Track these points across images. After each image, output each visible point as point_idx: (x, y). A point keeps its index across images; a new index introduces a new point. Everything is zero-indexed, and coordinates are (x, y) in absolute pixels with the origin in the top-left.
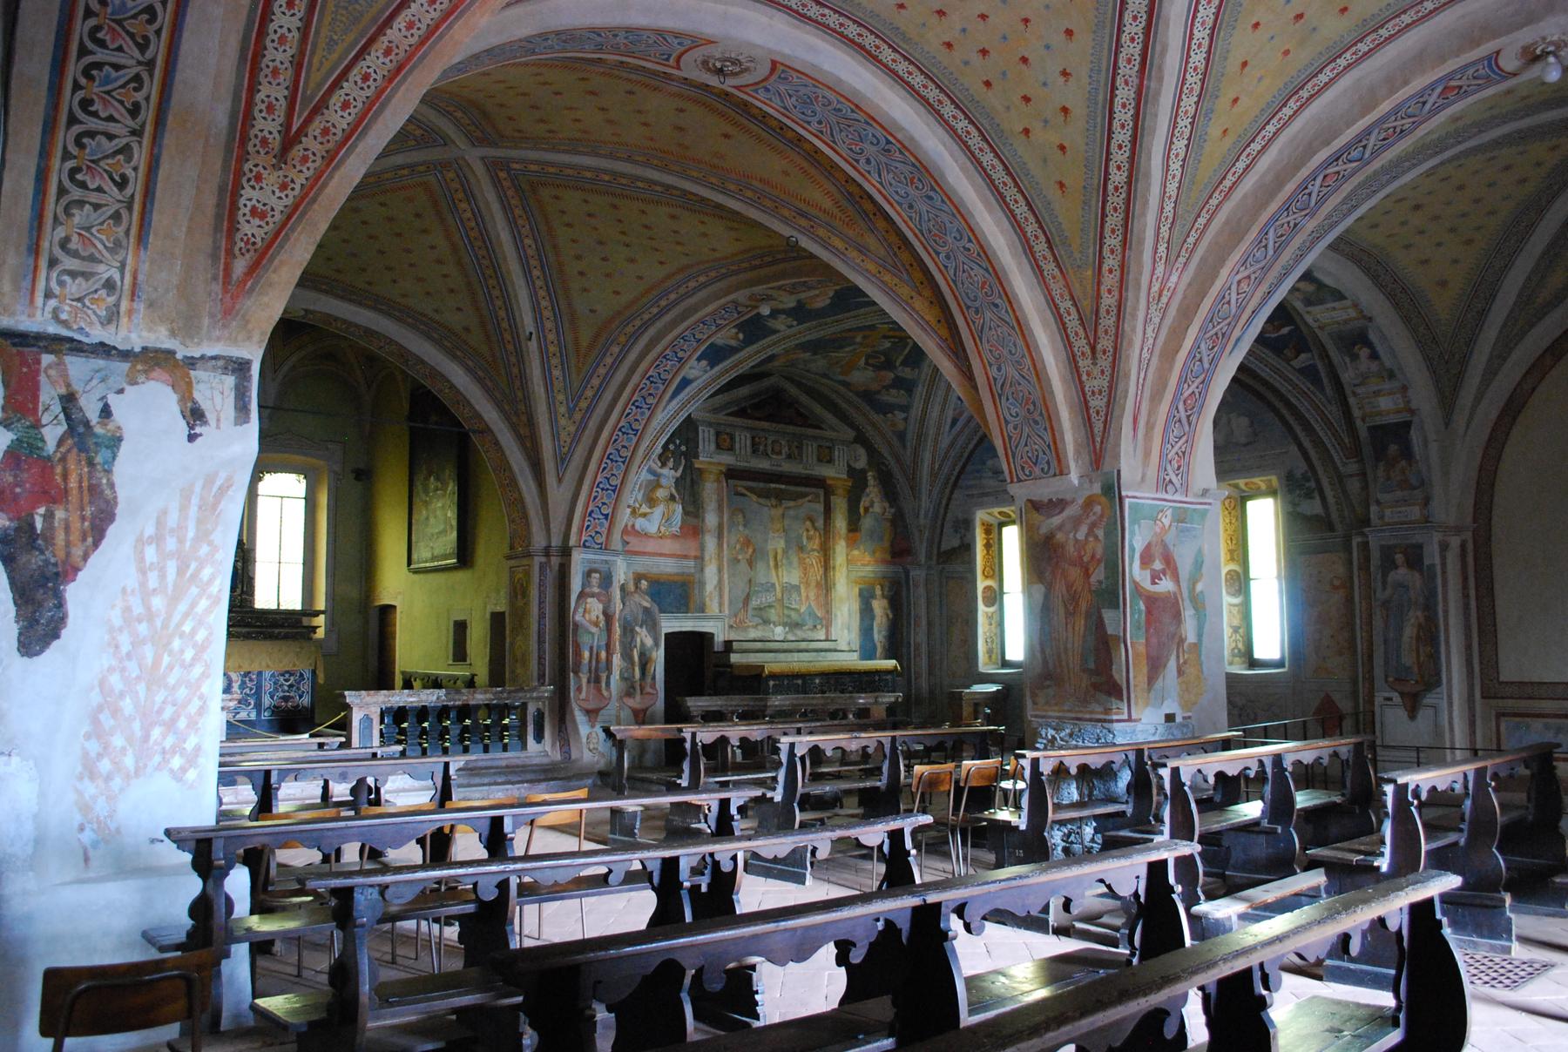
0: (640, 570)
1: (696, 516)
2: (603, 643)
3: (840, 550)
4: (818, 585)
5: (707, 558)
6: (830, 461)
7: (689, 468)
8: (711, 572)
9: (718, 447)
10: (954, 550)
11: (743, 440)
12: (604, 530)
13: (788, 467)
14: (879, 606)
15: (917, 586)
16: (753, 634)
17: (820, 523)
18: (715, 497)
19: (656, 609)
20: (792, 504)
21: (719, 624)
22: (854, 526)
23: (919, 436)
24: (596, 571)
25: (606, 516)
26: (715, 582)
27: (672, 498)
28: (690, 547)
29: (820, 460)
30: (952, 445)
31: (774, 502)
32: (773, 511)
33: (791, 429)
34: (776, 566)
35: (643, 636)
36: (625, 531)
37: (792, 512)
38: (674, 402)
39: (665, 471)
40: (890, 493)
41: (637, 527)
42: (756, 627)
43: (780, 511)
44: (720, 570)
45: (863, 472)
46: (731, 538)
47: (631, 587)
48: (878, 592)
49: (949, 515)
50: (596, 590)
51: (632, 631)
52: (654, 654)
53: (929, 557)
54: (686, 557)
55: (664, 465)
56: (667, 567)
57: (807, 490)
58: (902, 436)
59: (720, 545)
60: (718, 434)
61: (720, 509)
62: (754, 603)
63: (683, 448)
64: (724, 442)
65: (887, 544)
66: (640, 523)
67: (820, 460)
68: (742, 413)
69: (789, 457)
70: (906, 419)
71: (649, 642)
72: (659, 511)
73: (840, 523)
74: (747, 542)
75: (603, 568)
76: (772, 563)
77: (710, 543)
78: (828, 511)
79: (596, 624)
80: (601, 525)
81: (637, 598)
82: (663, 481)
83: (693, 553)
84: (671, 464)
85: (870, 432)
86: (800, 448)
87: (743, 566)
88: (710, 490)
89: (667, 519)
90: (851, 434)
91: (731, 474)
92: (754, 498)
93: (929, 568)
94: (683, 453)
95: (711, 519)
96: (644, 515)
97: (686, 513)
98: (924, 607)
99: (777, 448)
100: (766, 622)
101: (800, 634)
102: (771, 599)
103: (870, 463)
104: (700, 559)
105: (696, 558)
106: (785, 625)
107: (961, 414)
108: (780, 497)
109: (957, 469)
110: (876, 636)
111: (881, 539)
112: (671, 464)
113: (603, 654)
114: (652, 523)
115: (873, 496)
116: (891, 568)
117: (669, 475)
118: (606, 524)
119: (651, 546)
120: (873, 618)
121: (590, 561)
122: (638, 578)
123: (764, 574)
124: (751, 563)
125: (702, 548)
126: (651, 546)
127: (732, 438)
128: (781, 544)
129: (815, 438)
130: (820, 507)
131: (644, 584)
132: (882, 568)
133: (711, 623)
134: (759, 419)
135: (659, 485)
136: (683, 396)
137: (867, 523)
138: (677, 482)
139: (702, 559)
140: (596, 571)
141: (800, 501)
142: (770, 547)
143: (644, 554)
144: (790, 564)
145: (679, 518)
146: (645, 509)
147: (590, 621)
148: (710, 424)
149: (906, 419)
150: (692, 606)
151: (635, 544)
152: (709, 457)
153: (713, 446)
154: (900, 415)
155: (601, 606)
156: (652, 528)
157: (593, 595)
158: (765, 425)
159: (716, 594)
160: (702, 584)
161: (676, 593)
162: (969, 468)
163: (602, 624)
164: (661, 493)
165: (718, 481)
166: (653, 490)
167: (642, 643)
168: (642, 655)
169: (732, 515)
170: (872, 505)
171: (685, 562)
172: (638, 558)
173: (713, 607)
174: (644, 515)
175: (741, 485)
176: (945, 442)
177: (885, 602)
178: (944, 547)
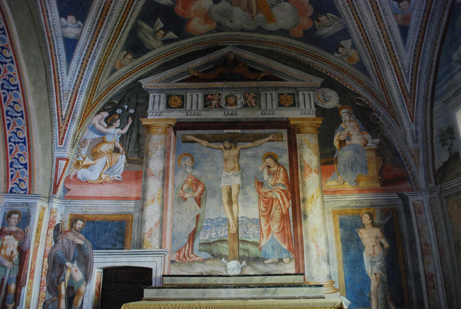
0: (78, 211)
1: (140, 163)
2: (14, 276)
3: (311, 183)
4: (284, 217)
5: (149, 197)
6: (294, 105)
7: (136, 125)
8: (152, 212)
9: (168, 106)
10: (446, 165)
11: (194, 99)
12: (26, 178)
13: (242, 115)
14: (370, 237)
15: (419, 211)
16: (199, 269)
17: (284, 159)
18: (160, 147)
19: (88, 245)
20: (249, 144)
21: (159, 260)
22: (328, 158)
23: (374, 58)
24: (15, 212)
25: (25, 165)
26: (156, 218)
27: (116, 150)
28: (132, 190)
29: (280, 105)
30: (417, 58)
31: (227, 144)
32: (226, 153)
33: (246, 84)
34: (230, 203)
35: (74, 271)
36: (68, 180)
37: (249, 152)
38: (74, 63)
39: (112, 130)
40: (368, 121)
41: (79, 176)
42: (203, 261)
43: (234, 152)
44: (163, 208)
45: (335, 111)
46: (178, 180)
47: (66, 226)
48: (366, 219)
49: (435, 131)
50: (14, 228)
51: (62, 267)
52: (83, 288)
53: (428, 180)
54: (126, 199)
55: (110, 125)
56: (106, 208)
57: (267, 131)
58: (361, 66)
59: (165, 186)
60: (168, 97)
61: (166, 156)
62: (201, 238)
63: (132, 111)
64: (174, 101)
65: (373, 171)
66: (82, 173)
67: (280, 105)
68: (193, 79)
69: (246, 106)
70: (353, 46)
71: (79, 276)
72: (101, 162)
73: (310, 156)
74: (197, 182)
75: (23, 209)
76: (225, 199)
77: (154, 186)
78: (293, 148)
79: (10, 259)
80: (23, 173)
81: (71, 236)
82: (109, 138)
83: (134, 195)
84: (118, 124)
85: (338, 76)
86: (257, 98)
87: (192, 204)
88: (156, 143)
89: (110, 168)
90: (318, 81)
91: (179, 126)
92: (205, 143)
93: (431, 191)
94: (131, 115)
95: (155, 164)
96: (87, 166)
97: (129, 161)
98: (432, 232)
99: (231, 100)
100: (217, 257)
101: (261, 268)
102: (223, 233)
103: (342, 102)
104: (141, 200)
105: (137, 199)
106: (240, 259)
107: (407, 18)
108: (234, 140)
109: (431, 81)
110: (368, 268)
111: (317, 154)
112: (118, 124)
113: (13, 287)
114: (94, 171)
115: (350, 131)
116: (380, 198)
117: (114, 133)
118: (27, 173)
119: (91, 191)
120: (361, 249)
121: (11, 204)
122: (74, 219)
123: (214, 209)
124: (199, 201)
125: (144, 190)
126: (91, 191)
127: (183, 98)
128: (236, 181)
129: (276, 88)
130: (285, 145)
131: (80, 224)
132: (367, 198)
133: (149, 258)
134: (214, 80)
135: (103, 141)
136: (76, 56)
137: (344, 155)
138: (122, 138)
139: (144, 199)
140: (15, 212)
141: (257, 142)
142: (224, 184)
143: (88, 198)
144: (247, 199)
145: (122, 166)
146: (88, 161)
147: (5, 256)
148: (161, 91)
149: (353, 46)
150: (128, 241)
151: (76, 190)
152: (158, 114)
153: (163, 107)
154: (347, 43)
155: (16, 243)
156: (93, 175)
157: (11, 233)
158: (218, 84)
159: (157, 231)
160: (141, 222)
161: (116, 232)
162: (440, 73)
163: (16, 258)
164: (105, 148)
165: (166, 132)
166: (97, 145)
167: (71, 277)
168: (70, 289)
169: (178, 160)
170: (349, 137)
171: (125, 203)
172: (78, 202)
173: (153, 242)
174: (87, 166)
175: (189, 134)
176: (406, 57)
177: (377, 232)
178: (438, 166)
